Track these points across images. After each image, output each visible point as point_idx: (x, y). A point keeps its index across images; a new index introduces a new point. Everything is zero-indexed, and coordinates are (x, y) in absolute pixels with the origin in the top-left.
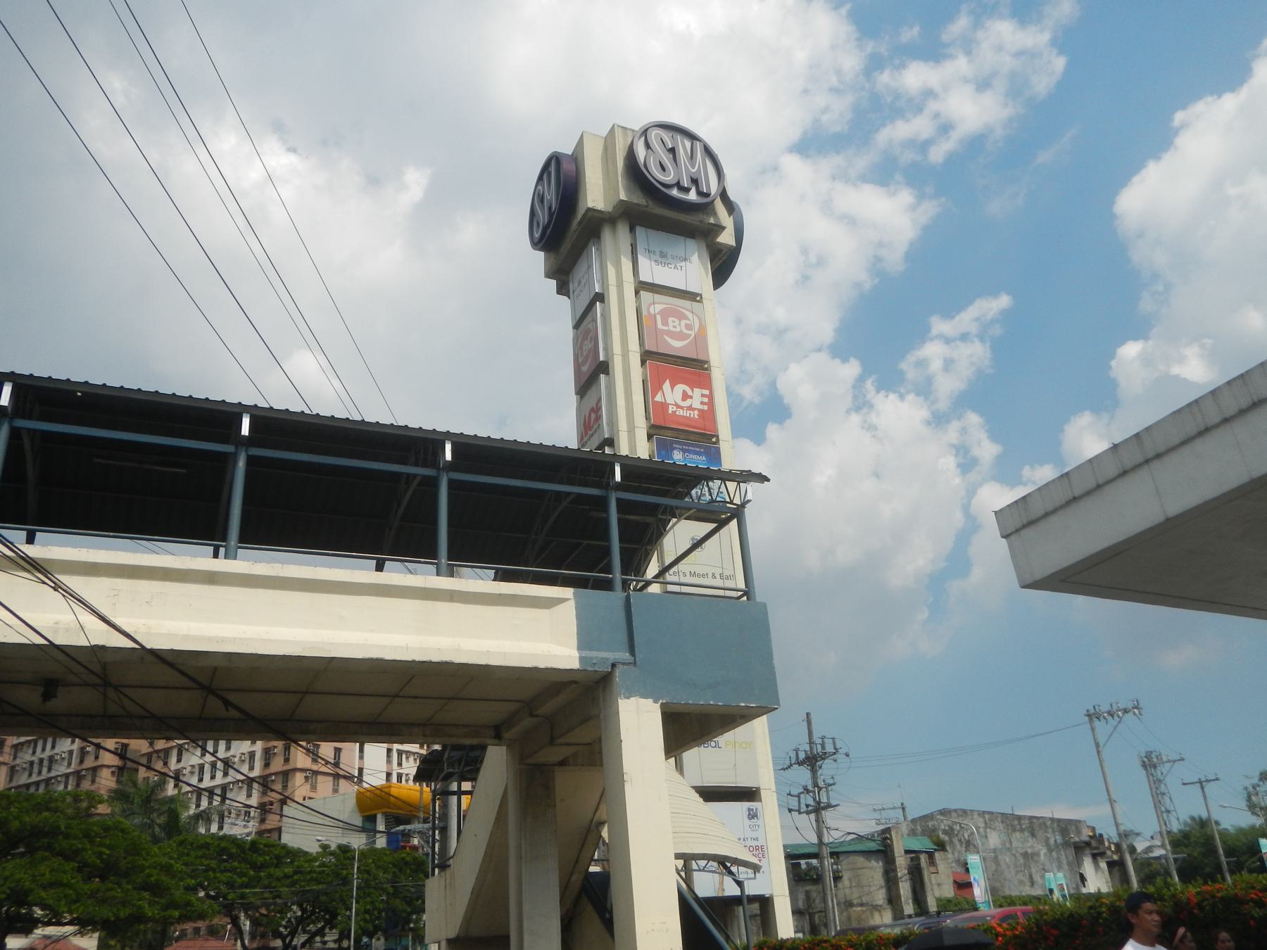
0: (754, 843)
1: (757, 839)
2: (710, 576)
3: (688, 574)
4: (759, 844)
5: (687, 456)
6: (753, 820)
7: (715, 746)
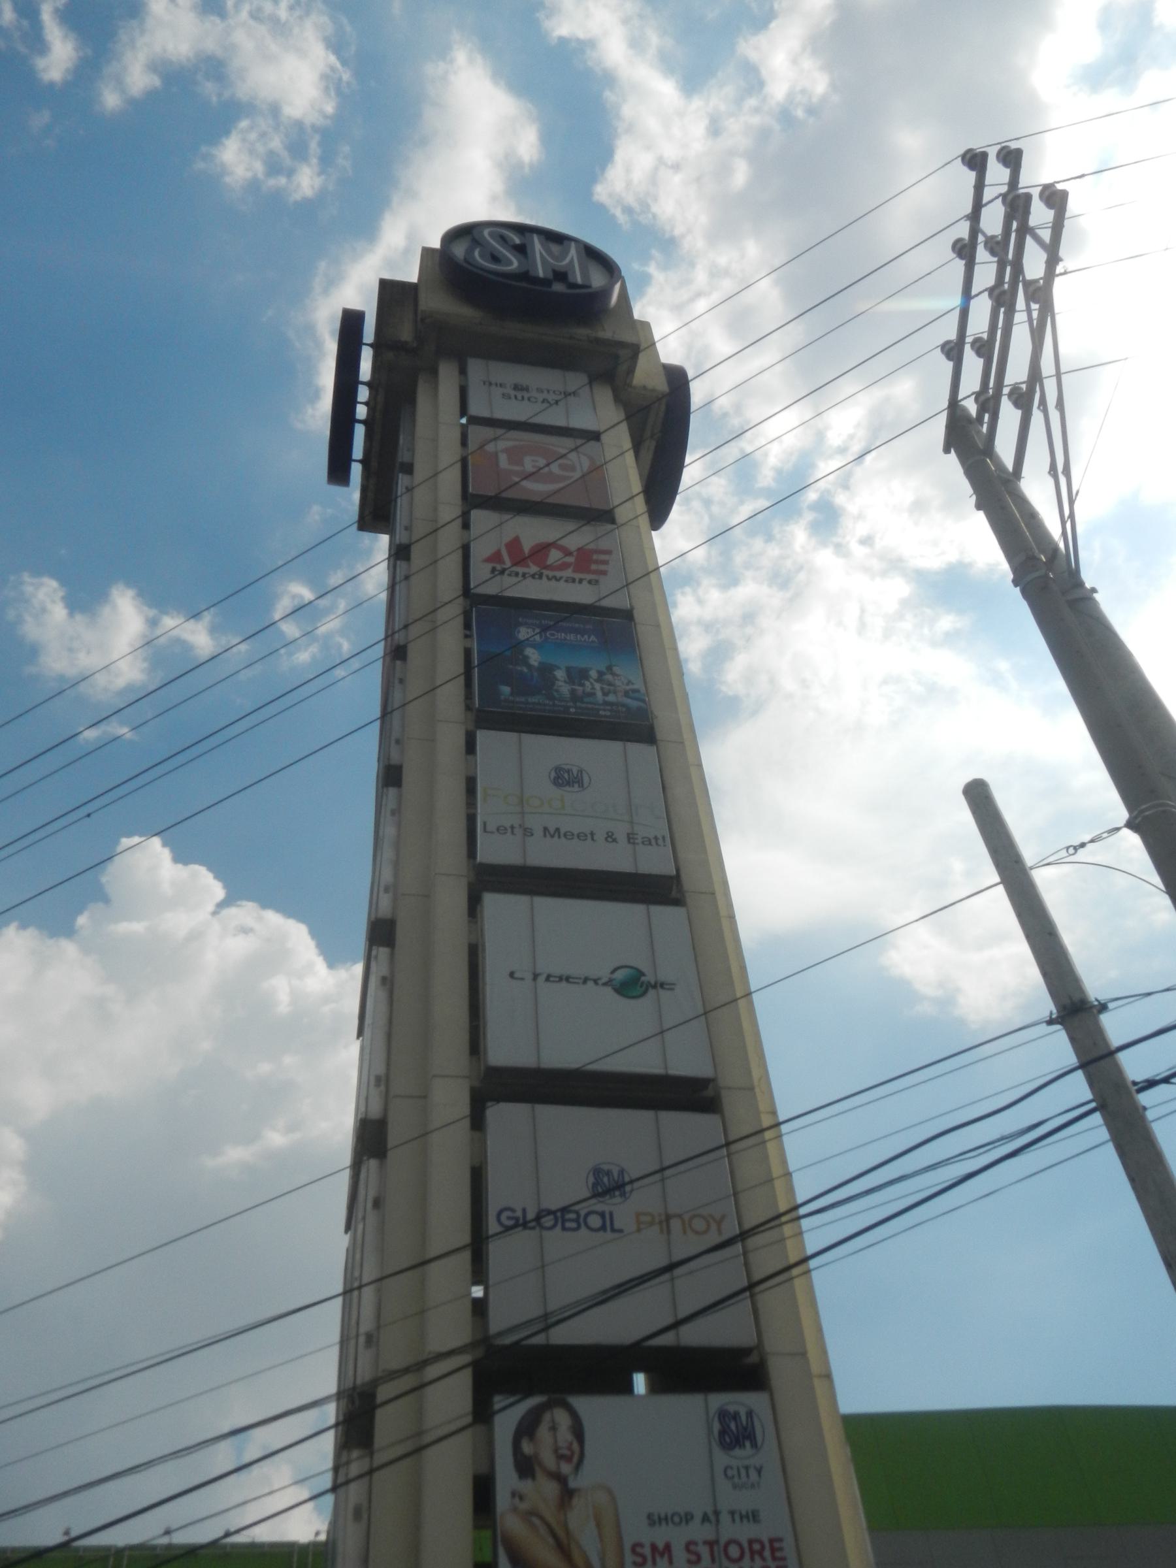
0: (745, 1532)
1: (753, 1516)
2: (600, 836)
3: (538, 832)
4: (763, 1532)
5: (553, 635)
6: (737, 1452)
7: (603, 1228)
